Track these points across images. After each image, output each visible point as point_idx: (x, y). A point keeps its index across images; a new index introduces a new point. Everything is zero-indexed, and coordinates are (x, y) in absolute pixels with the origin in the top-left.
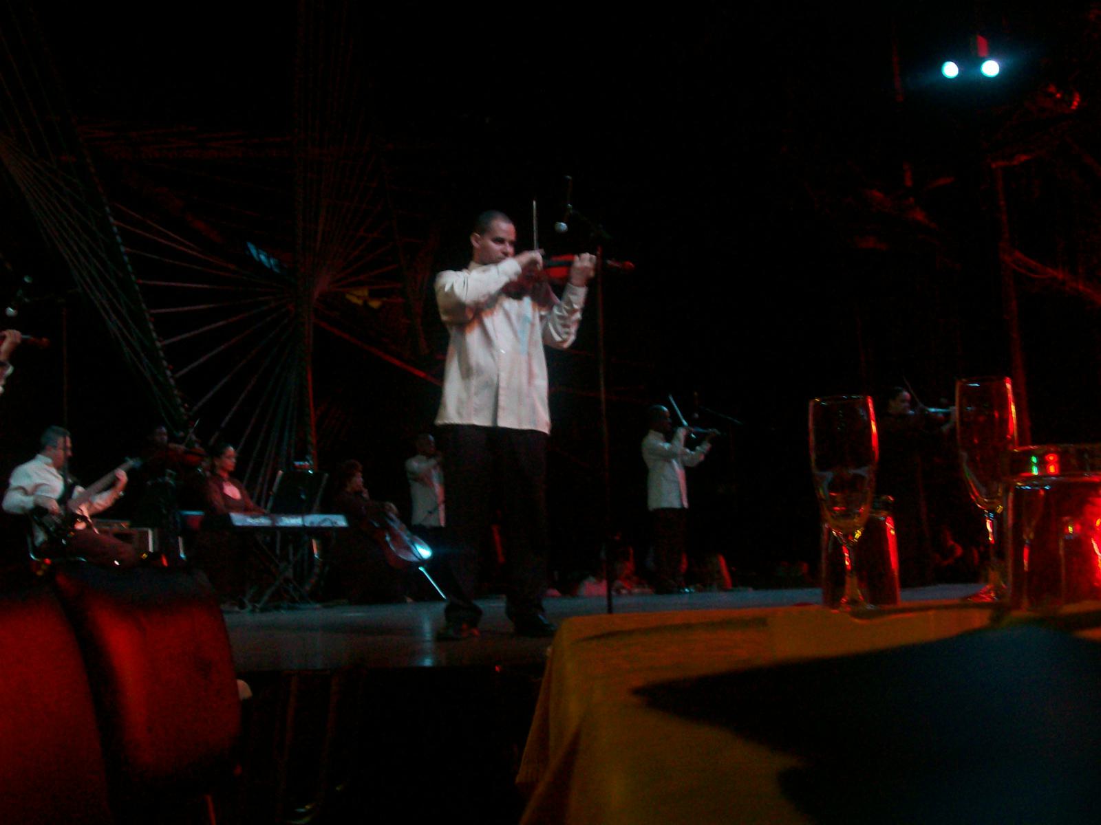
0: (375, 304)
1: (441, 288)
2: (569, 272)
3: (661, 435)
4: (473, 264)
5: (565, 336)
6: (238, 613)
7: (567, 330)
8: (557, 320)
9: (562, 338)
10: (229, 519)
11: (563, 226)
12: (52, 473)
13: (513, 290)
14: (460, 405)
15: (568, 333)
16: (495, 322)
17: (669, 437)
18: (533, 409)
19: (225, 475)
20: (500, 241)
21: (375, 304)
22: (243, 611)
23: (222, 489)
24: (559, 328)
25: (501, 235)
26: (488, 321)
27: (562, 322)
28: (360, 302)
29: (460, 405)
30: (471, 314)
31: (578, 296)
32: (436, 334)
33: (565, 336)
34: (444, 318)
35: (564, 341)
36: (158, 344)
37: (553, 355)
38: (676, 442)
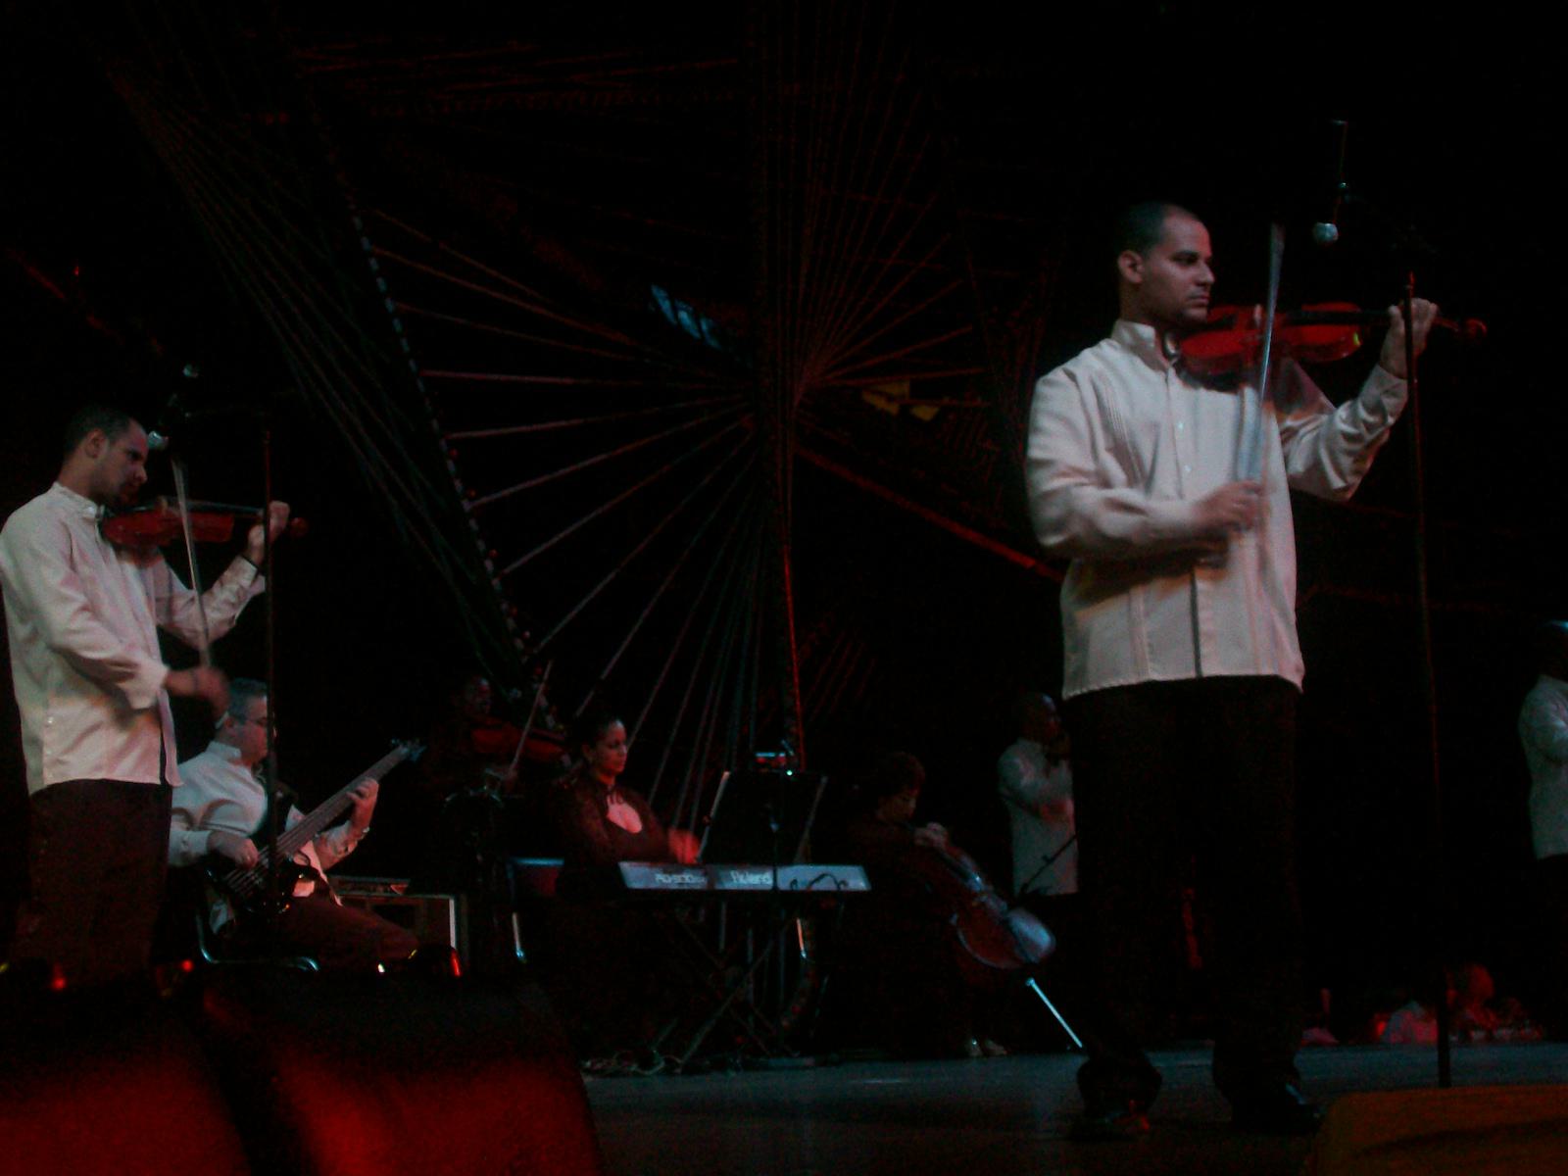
0: (925, 412)
6: (636, 1074)
8: (1343, 444)
9: (1346, 481)
10: (618, 878)
11: (1330, 230)
18: (1276, 642)
19: (611, 782)
20: (1189, 259)
21: (925, 412)
22: (646, 1073)
23: (605, 810)
25: (1187, 246)
27: (1357, 447)
28: (893, 409)
31: (1386, 394)
36: (467, 506)
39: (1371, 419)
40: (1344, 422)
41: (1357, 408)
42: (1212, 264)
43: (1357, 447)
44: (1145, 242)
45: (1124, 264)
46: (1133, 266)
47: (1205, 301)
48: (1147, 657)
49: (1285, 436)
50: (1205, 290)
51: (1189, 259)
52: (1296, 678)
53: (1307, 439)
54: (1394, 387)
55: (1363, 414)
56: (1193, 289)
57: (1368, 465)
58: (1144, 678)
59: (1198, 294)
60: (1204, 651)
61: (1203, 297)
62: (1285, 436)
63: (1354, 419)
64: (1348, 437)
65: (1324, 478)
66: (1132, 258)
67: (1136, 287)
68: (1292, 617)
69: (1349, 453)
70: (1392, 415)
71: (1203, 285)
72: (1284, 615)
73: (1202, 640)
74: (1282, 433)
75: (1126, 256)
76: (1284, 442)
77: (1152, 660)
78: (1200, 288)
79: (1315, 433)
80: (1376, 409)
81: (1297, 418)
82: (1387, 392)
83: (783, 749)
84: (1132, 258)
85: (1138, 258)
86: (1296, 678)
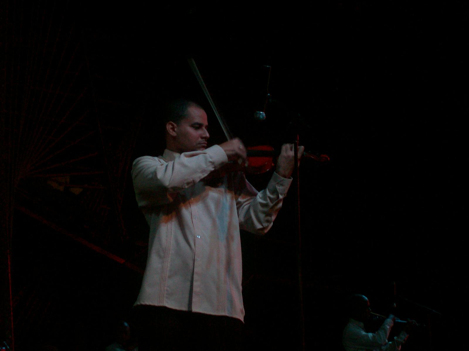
0: (77, 191)
1: (140, 172)
2: (275, 161)
3: (362, 324)
4: (166, 151)
5: (265, 225)
7: (269, 218)
8: (260, 208)
9: (262, 225)
11: (262, 114)
12: (149, 159)
13: (214, 179)
14: (160, 289)
15: (268, 221)
16: (195, 213)
17: (373, 326)
18: (231, 302)
20: (198, 126)
21: (77, 191)
24: (262, 216)
25: (198, 120)
26: (185, 212)
27: (265, 209)
28: (61, 188)
29: (160, 289)
30: (172, 201)
32: (138, 216)
33: (265, 225)
34: (141, 204)
35: (264, 228)
37: (249, 237)
38: (381, 332)
39: (271, 196)
40: (261, 198)
41: (266, 191)
42: (208, 128)
43: (265, 209)
44: (178, 117)
45: (169, 127)
46: (173, 129)
47: (206, 145)
48: (165, 295)
49: (238, 206)
50: (206, 141)
51: (198, 126)
52: (240, 315)
53: (246, 207)
54: (281, 181)
55: (268, 193)
56: (200, 139)
57: (273, 218)
58: (161, 304)
59: (203, 142)
60: (194, 300)
61: (205, 144)
62: (238, 206)
63: (264, 197)
64: (263, 205)
65: (252, 223)
66: (173, 125)
67: (174, 138)
68: (241, 288)
69: (264, 212)
70: (281, 194)
71: (205, 138)
72: (237, 288)
73: (194, 295)
74: (237, 204)
75: (170, 124)
76: (238, 209)
77: (167, 298)
78: (204, 140)
79: (248, 205)
80: (274, 191)
81: (243, 198)
82: (278, 183)
83: (4, 346)
84: (173, 125)
85: (175, 125)
86: (240, 315)
